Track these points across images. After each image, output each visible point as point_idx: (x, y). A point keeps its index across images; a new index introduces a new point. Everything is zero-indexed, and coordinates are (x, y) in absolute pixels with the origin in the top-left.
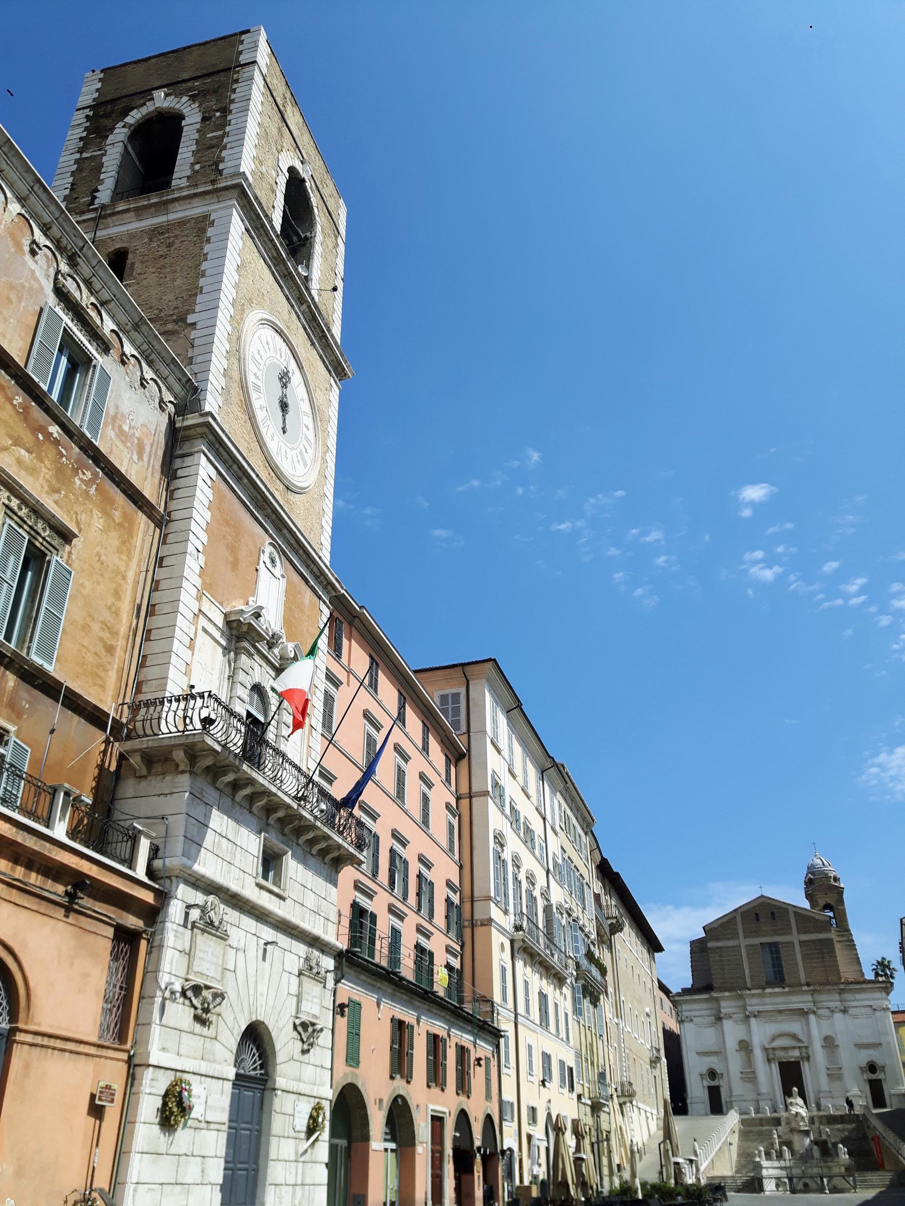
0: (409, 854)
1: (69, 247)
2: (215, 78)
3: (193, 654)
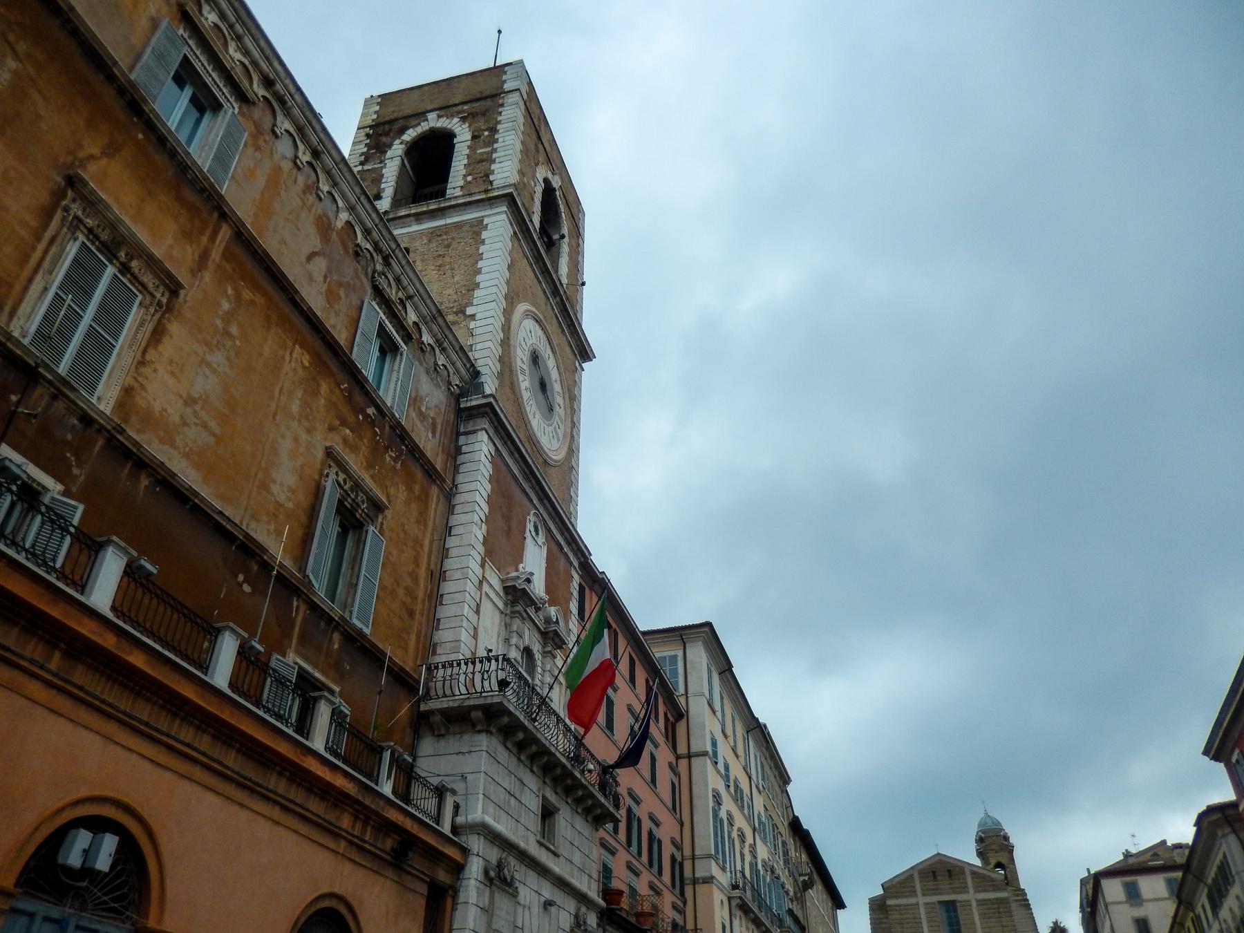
0: (641, 812)
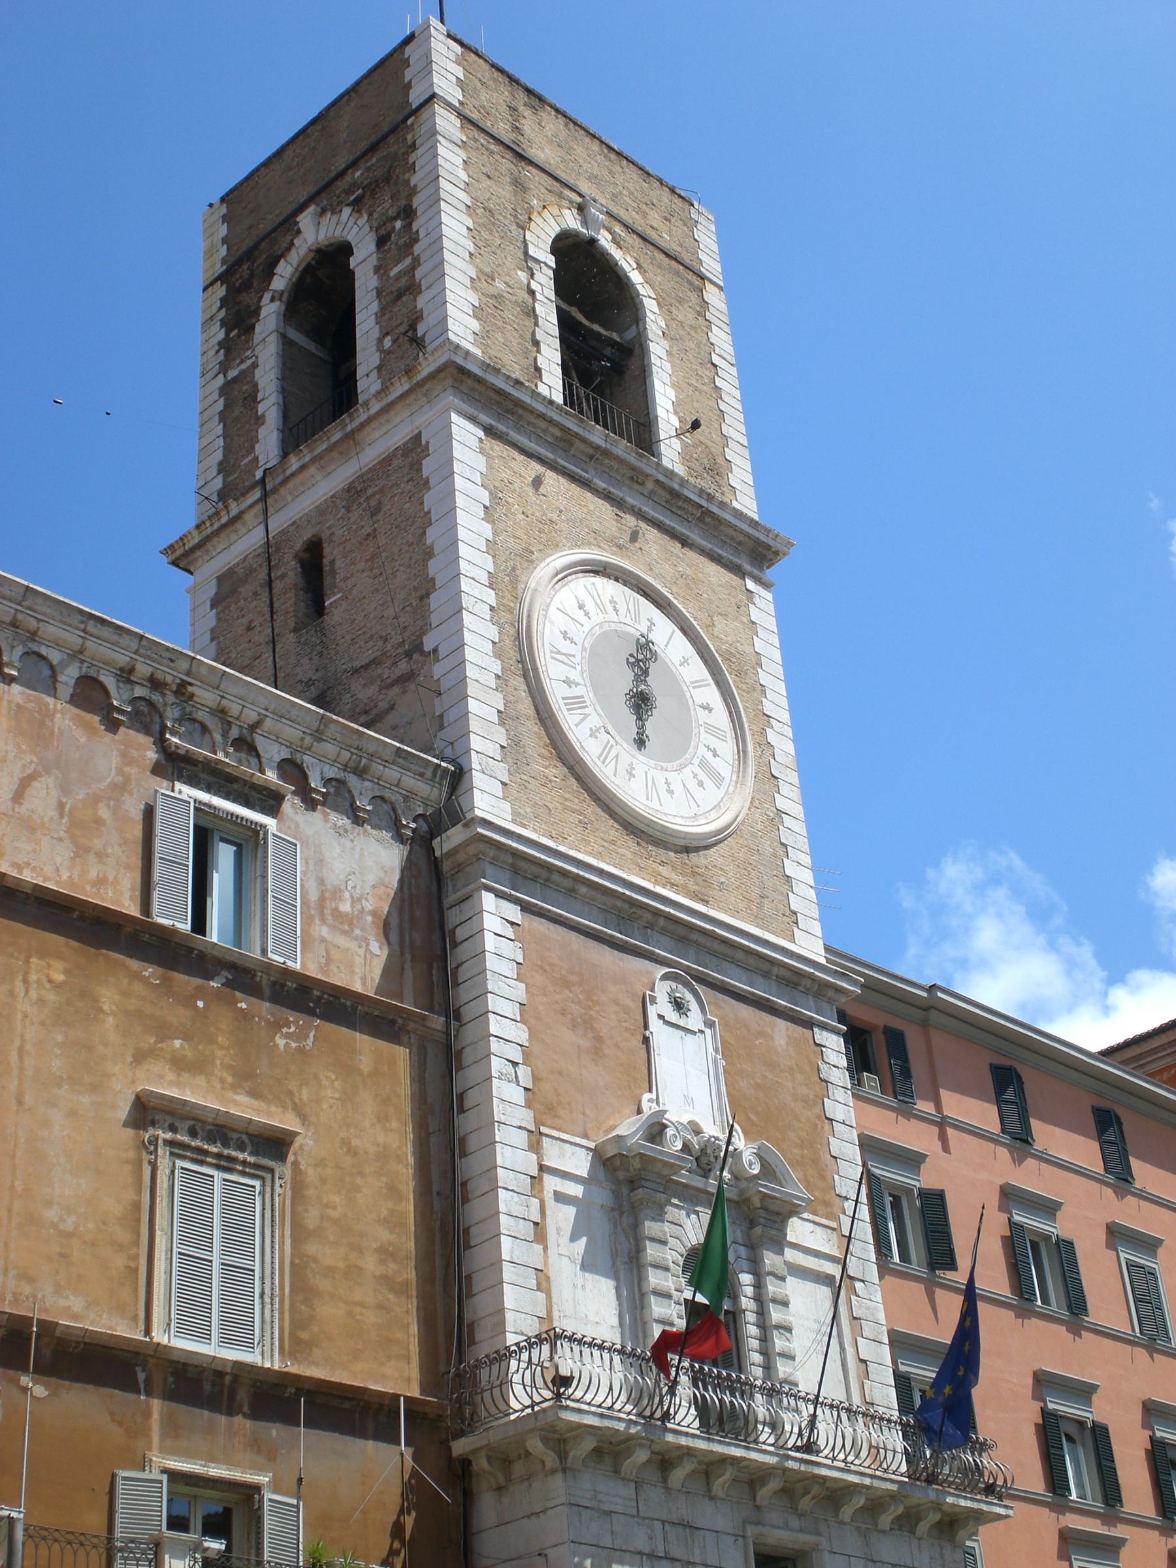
1: (169, 679)
2: (382, 153)
3: (545, 1249)
